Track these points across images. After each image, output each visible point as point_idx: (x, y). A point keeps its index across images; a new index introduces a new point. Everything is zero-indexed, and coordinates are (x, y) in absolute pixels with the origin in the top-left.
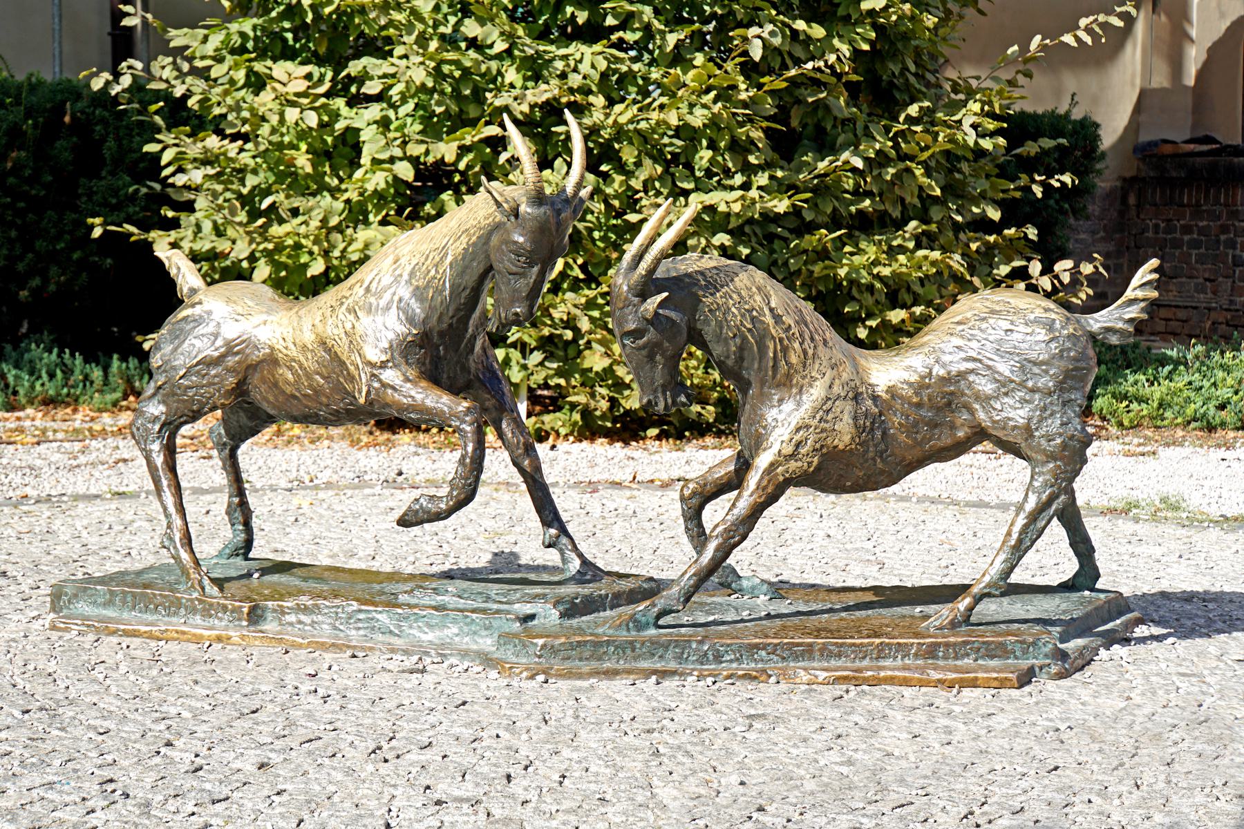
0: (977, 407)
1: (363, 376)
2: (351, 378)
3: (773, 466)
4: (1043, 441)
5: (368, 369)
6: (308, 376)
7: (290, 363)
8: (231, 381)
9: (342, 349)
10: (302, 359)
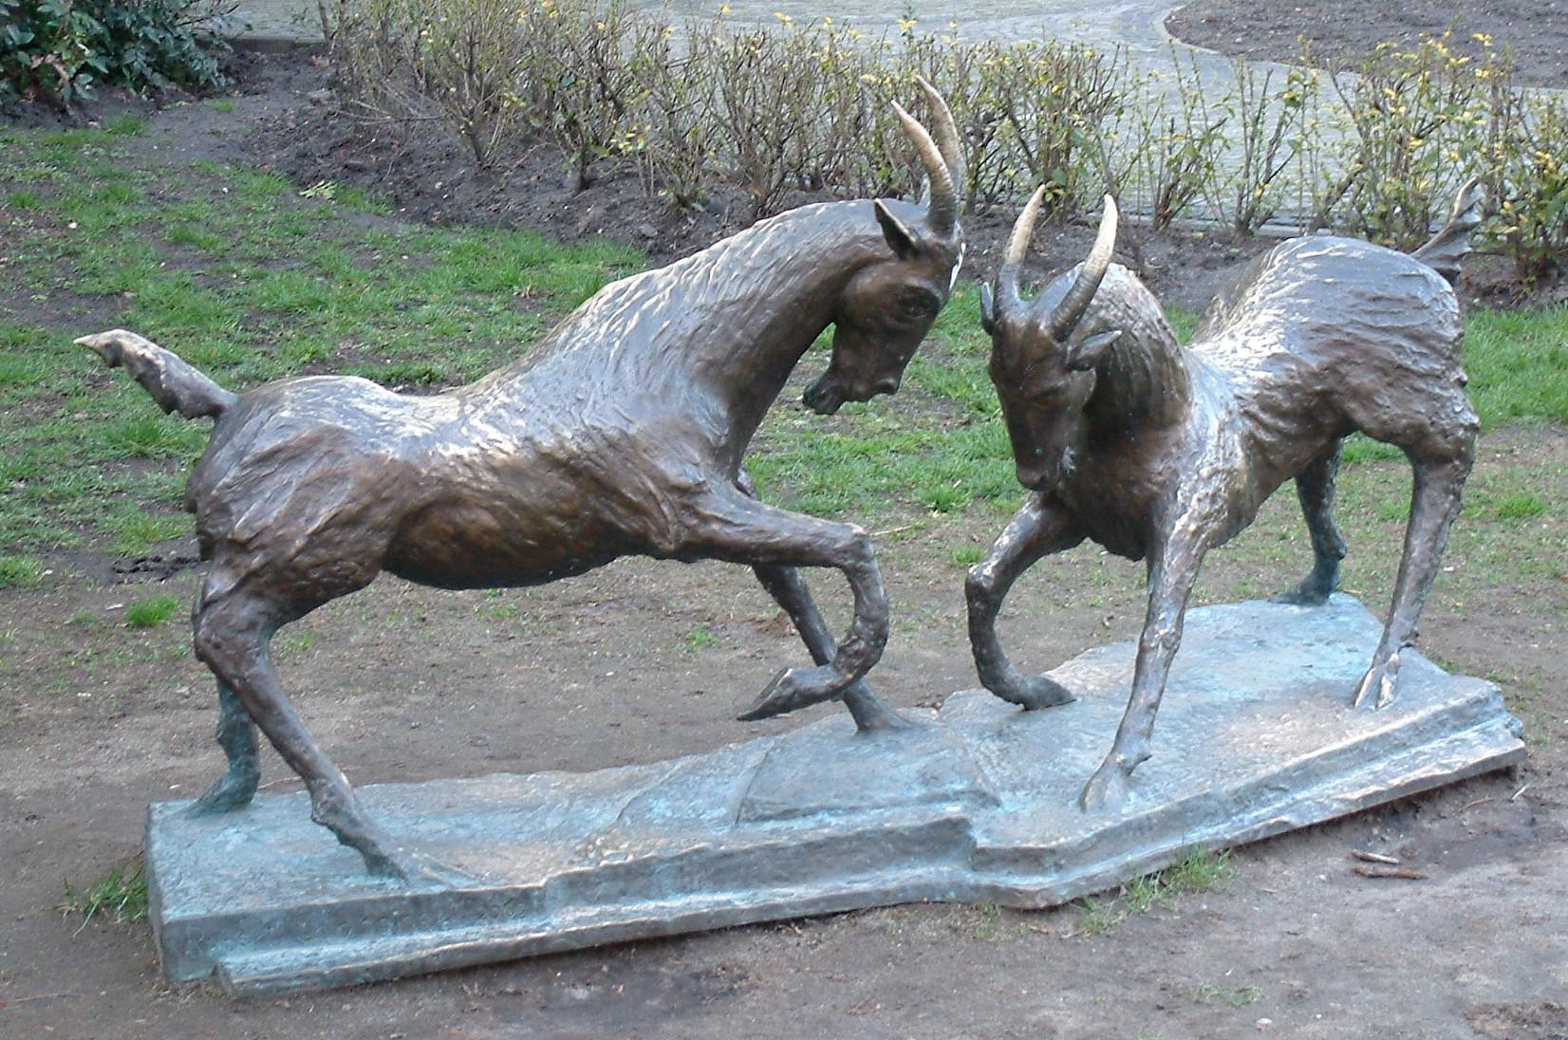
0: (1353, 405)
1: (665, 509)
4: (1439, 438)
5: (674, 497)
10: (516, 494)
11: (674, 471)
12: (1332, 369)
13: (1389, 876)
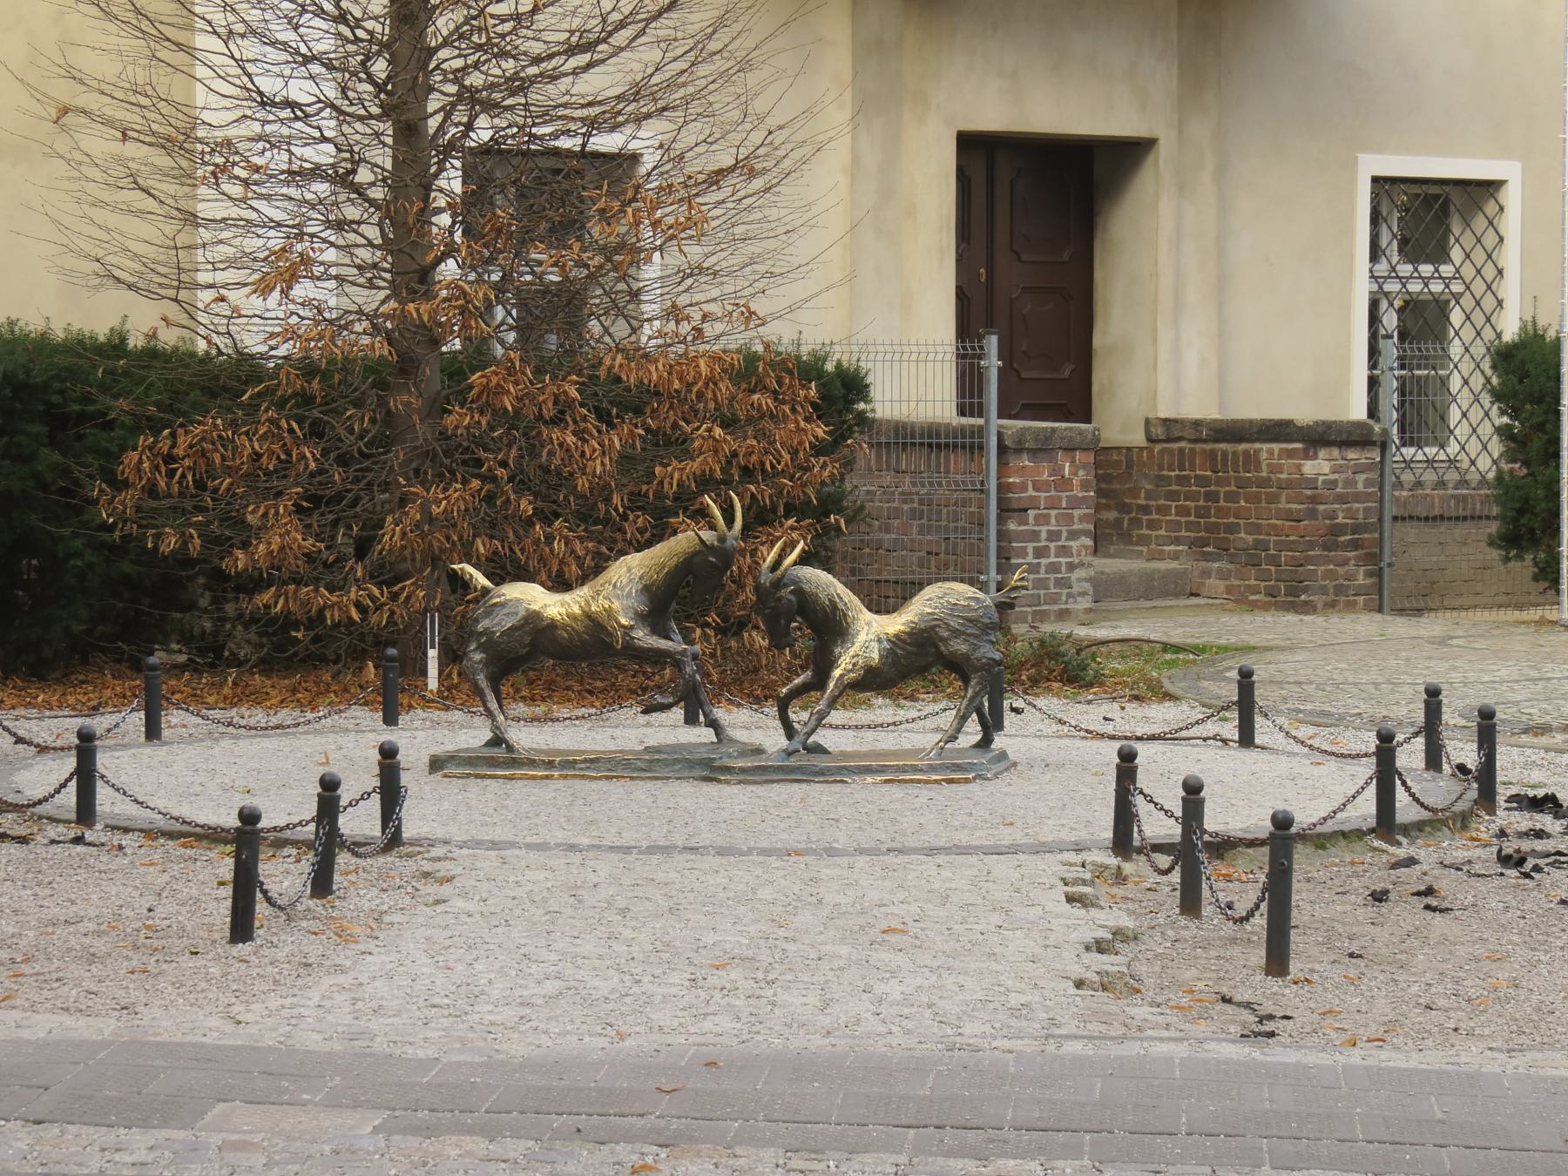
2: (610, 635)
3: (842, 676)
6: (578, 634)
7: (565, 627)
8: (528, 639)
11: (624, 621)
13: (743, 770)
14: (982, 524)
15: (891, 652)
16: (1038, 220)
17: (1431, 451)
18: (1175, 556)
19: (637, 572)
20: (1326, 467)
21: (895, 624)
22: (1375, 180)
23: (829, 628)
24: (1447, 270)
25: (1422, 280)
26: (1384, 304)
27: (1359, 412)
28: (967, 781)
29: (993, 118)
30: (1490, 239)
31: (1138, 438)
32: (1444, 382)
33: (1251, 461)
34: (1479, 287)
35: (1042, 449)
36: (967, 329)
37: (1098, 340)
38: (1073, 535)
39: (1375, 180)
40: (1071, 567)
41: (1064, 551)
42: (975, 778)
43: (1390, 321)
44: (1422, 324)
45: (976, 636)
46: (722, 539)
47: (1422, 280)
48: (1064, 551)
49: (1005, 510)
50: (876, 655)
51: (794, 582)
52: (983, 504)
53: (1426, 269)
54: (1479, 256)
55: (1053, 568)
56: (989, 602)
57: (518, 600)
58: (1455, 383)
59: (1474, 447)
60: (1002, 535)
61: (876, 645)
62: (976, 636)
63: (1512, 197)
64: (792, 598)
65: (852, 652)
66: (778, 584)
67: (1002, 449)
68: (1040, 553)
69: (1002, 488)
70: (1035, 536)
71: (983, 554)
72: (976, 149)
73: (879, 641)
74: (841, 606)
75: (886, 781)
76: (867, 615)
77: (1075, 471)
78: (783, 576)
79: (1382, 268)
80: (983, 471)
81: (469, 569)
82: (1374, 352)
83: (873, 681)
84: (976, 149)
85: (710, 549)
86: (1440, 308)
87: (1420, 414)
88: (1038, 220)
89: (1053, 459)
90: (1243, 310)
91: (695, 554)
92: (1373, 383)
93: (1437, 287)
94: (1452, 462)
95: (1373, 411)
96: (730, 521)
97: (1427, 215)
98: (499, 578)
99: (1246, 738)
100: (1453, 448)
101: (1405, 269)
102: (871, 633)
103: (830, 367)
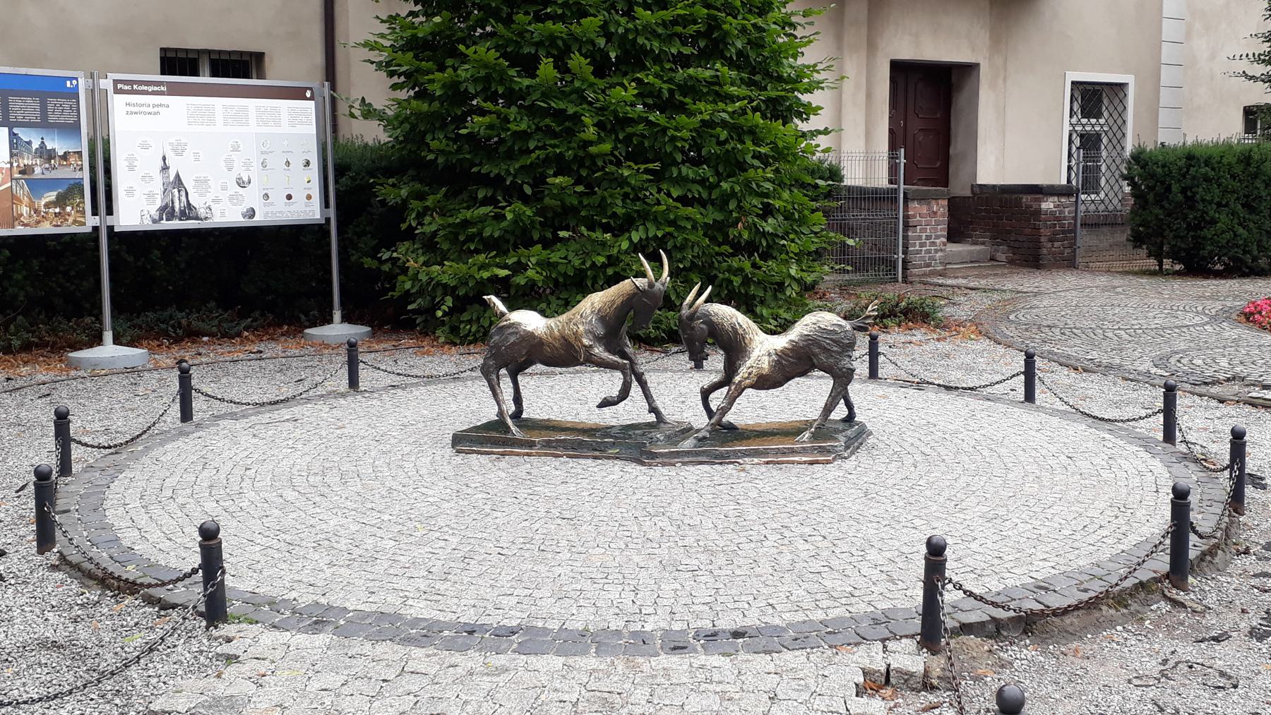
9: (572, 340)
11: (586, 342)
12: (808, 345)
14: (896, 233)
15: (778, 363)
16: (930, 101)
17: (1093, 196)
18: (983, 244)
19: (597, 306)
20: (1052, 206)
21: (780, 342)
22: (1073, 83)
23: (734, 348)
24: (1102, 121)
25: (1091, 125)
26: (1074, 136)
27: (1064, 182)
28: (828, 462)
29: (907, 53)
30: (1120, 108)
31: (968, 193)
32: (1099, 167)
33: (1018, 203)
34: (1115, 128)
35: (923, 198)
36: (893, 147)
37: (951, 151)
38: (937, 237)
39: (1073, 83)
40: (936, 251)
41: (933, 244)
42: (834, 459)
43: (1077, 142)
44: (1089, 143)
45: (839, 353)
46: (651, 285)
47: (1091, 125)
48: (933, 244)
49: (907, 226)
50: (766, 366)
51: (705, 316)
52: (897, 224)
53: (1093, 121)
54: (1115, 115)
55: (928, 252)
56: (848, 327)
57: (519, 324)
58: (1103, 168)
59: (1111, 195)
60: (906, 238)
61: (766, 358)
62: (839, 353)
63: (1131, 92)
64: (704, 326)
65: (748, 364)
66: (692, 317)
67: (905, 198)
68: (922, 245)
69: (906, 217)
70: (920, 238)
71: (896, 246)
72: (900, 69)
73: (769, 355)
74: (740, 331)
75: (767, 463)
76: (762, 336)
77: (941, 207)
78: (696, 312)
79: (1074, 120)
80: (897, 209)
81: (494, 299)
82: (1070, 155)
83: (764, 382)
84: (900, 69)
85: (643, 292)
86: (1098, 137)
87: (1090, 181)
88: (930, 101)
89: (929, 204)
90: (1016, 142)
91: (634, 295)
92: (1070, 168)
93: (1097, 128)
94: (1102, 201)
95: (1069, 181)
96: (658, 276)
97: (1092, 98)
98: (512, 308)
99: (1030, 396)
100: (1102, 195)
101: (1084, 121)
102: (764, 347)
103: (826, 165)
